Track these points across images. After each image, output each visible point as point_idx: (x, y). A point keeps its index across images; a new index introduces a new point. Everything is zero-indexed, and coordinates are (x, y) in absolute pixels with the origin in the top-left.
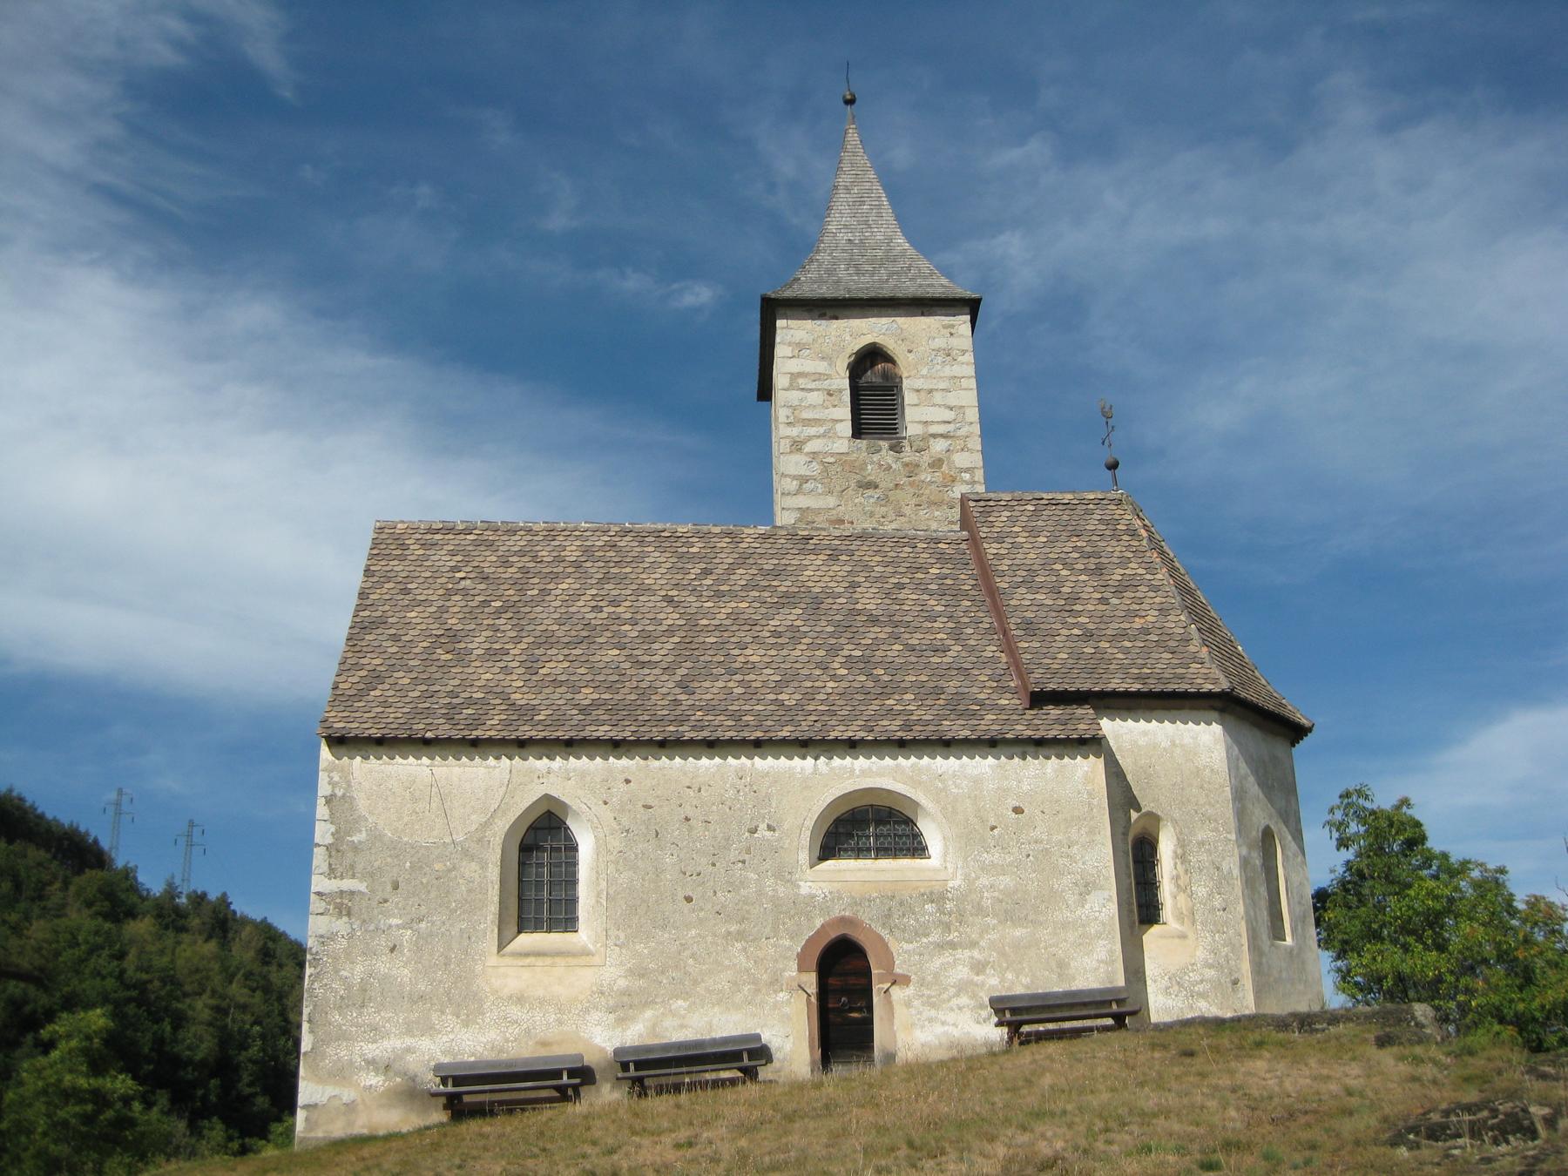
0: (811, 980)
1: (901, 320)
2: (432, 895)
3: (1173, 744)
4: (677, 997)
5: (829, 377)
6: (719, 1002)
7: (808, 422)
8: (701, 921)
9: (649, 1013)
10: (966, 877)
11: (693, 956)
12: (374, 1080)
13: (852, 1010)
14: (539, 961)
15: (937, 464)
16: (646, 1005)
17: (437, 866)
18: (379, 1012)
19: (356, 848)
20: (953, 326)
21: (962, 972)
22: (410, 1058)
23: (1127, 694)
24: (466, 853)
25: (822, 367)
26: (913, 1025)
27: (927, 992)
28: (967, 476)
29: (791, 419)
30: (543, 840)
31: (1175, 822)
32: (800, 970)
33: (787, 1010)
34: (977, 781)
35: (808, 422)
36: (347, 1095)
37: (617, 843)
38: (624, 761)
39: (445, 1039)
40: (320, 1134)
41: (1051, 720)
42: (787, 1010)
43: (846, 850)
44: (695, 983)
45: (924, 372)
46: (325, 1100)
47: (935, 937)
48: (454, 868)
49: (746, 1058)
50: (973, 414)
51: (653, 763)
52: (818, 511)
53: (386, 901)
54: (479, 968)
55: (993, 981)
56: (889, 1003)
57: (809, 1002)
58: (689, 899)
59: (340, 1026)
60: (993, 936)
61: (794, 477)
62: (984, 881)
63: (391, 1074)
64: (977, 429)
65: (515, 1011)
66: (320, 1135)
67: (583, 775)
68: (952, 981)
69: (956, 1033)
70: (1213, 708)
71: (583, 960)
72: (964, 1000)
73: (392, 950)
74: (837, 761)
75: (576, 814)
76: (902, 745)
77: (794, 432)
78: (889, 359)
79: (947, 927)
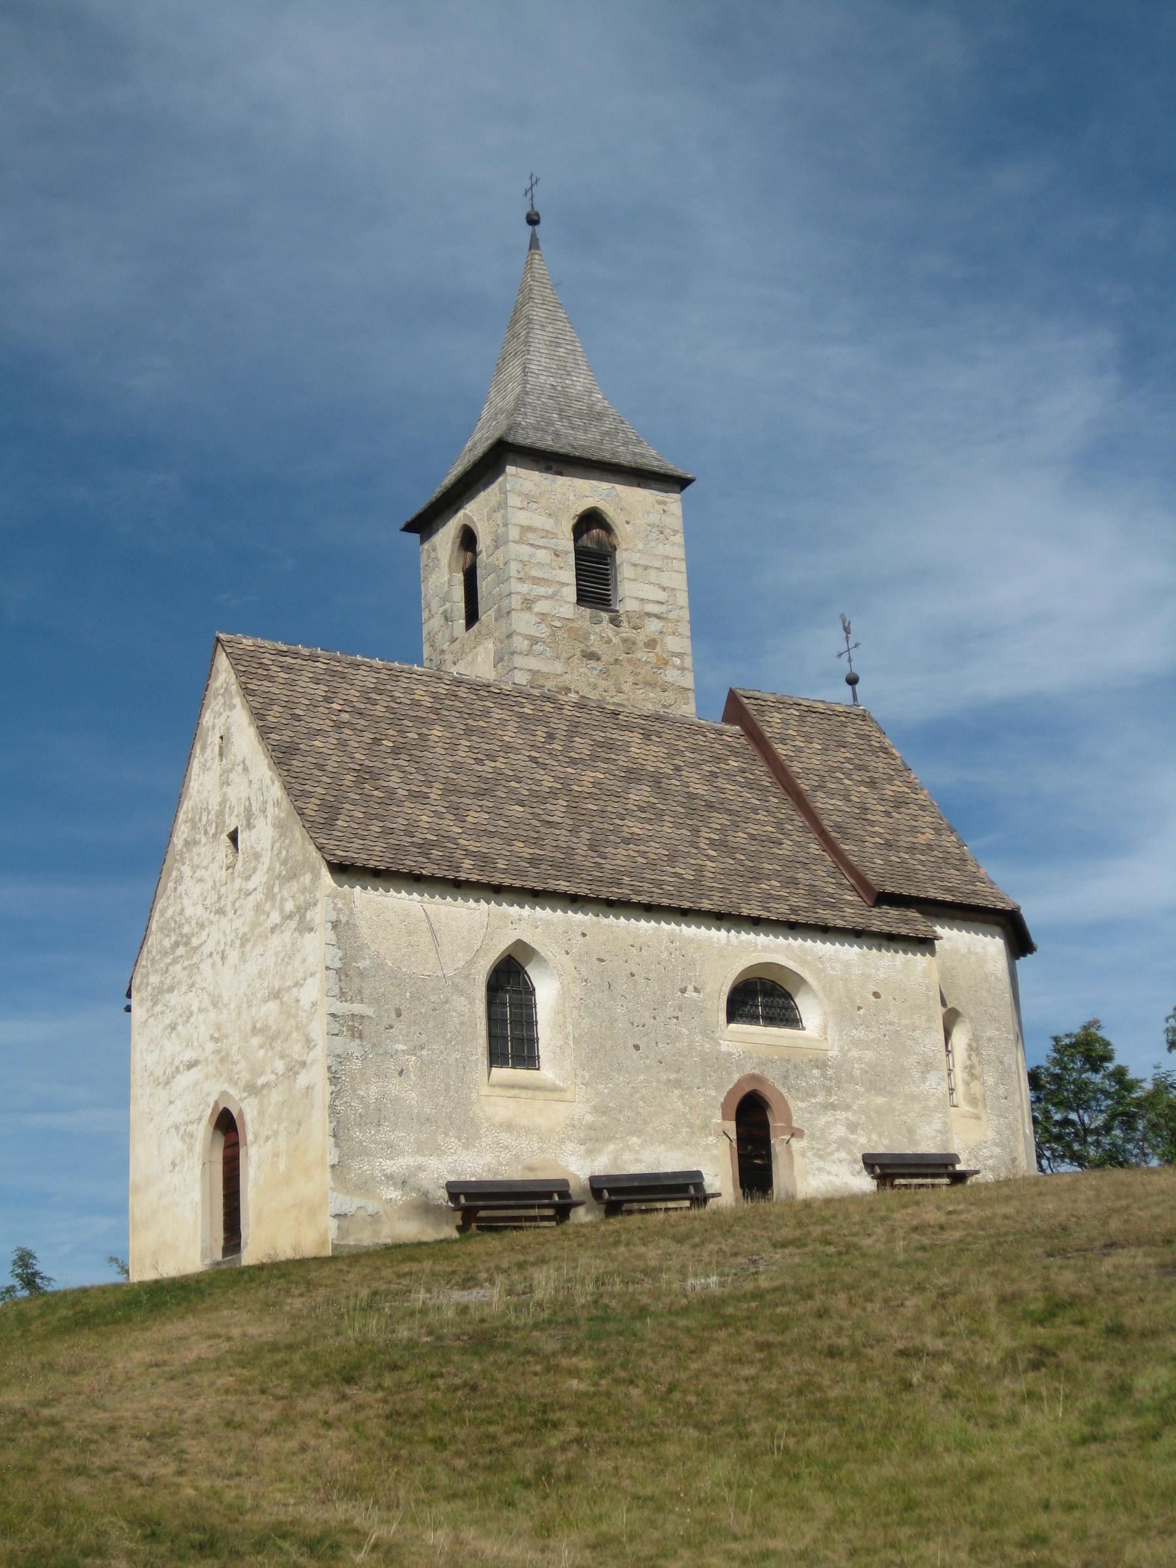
0: (731, 1127)
1: (620, 488)
2: (430, 1025)
3: (969, 952)
4: (632, 1134)
5: (555, 536)
6: (664, 1141)
7: (537, 581)
8: (648, 1068)
9: (611, 1147)
10: (841, 1048)
11: (642, 1098)
12: (393, 1194)
13: (756, 1157)
14: (523, 1094)
15: (651, 644)
16: (609, 1139)
17: (433, 998)
18: (393, 1131)
19: (361, 974)
20: (665, 503)
21: (840, 1131)
22: (422, 1175)
23: (944, 904)
24: (455, 986)
25: (549, 524)
26: (807, 1172)
27: (817, 1146)
28: (677, 661)
29: (521, 575)
30: (509, 980)
31: (971, 1019)
32: (724, 1118)
33: (715, 1152)
34: (847, 965)
35: (537, 581)
36: (372, 1206)
37: (578, 991)
38: (580, 916)
39: (450, 1159)
40: (351, 1242)
41: (889, 919)
42: (715, 1152)
43: (741, 1016)
44: (645, 1122)
45: (641, 546)
46: (353, 1210)
47: (820, 1099)
48: (447, 1002)
49: (685, 1187)
50: (683, 599)
51: (604, 921)
52: (547, 676)
53: (391, 1027)
54: (474, 1096)
55: (863, 1140)
56: (790, 1153)
57: (731, 1145)
58: (637, 1047)
59: (361, 1142)
60: (862, 1102)
61: (526, 637)
62: (854, 1053)
63: (407, 1189)
64: (686, 614)
65: (505, 1138)
66: (352, 1243)
67: (548, 924)
68: (833, 1137)
69: (838, 1182)
70: (998, 924)
71: (557, 1095)
72: (843, 1155)
73: (401, 1073)
74: (743, 936)
75: (543, 961)
76: (792, 927)
77: (524, 588)
78: (607, 527)
79: (829, 1091)
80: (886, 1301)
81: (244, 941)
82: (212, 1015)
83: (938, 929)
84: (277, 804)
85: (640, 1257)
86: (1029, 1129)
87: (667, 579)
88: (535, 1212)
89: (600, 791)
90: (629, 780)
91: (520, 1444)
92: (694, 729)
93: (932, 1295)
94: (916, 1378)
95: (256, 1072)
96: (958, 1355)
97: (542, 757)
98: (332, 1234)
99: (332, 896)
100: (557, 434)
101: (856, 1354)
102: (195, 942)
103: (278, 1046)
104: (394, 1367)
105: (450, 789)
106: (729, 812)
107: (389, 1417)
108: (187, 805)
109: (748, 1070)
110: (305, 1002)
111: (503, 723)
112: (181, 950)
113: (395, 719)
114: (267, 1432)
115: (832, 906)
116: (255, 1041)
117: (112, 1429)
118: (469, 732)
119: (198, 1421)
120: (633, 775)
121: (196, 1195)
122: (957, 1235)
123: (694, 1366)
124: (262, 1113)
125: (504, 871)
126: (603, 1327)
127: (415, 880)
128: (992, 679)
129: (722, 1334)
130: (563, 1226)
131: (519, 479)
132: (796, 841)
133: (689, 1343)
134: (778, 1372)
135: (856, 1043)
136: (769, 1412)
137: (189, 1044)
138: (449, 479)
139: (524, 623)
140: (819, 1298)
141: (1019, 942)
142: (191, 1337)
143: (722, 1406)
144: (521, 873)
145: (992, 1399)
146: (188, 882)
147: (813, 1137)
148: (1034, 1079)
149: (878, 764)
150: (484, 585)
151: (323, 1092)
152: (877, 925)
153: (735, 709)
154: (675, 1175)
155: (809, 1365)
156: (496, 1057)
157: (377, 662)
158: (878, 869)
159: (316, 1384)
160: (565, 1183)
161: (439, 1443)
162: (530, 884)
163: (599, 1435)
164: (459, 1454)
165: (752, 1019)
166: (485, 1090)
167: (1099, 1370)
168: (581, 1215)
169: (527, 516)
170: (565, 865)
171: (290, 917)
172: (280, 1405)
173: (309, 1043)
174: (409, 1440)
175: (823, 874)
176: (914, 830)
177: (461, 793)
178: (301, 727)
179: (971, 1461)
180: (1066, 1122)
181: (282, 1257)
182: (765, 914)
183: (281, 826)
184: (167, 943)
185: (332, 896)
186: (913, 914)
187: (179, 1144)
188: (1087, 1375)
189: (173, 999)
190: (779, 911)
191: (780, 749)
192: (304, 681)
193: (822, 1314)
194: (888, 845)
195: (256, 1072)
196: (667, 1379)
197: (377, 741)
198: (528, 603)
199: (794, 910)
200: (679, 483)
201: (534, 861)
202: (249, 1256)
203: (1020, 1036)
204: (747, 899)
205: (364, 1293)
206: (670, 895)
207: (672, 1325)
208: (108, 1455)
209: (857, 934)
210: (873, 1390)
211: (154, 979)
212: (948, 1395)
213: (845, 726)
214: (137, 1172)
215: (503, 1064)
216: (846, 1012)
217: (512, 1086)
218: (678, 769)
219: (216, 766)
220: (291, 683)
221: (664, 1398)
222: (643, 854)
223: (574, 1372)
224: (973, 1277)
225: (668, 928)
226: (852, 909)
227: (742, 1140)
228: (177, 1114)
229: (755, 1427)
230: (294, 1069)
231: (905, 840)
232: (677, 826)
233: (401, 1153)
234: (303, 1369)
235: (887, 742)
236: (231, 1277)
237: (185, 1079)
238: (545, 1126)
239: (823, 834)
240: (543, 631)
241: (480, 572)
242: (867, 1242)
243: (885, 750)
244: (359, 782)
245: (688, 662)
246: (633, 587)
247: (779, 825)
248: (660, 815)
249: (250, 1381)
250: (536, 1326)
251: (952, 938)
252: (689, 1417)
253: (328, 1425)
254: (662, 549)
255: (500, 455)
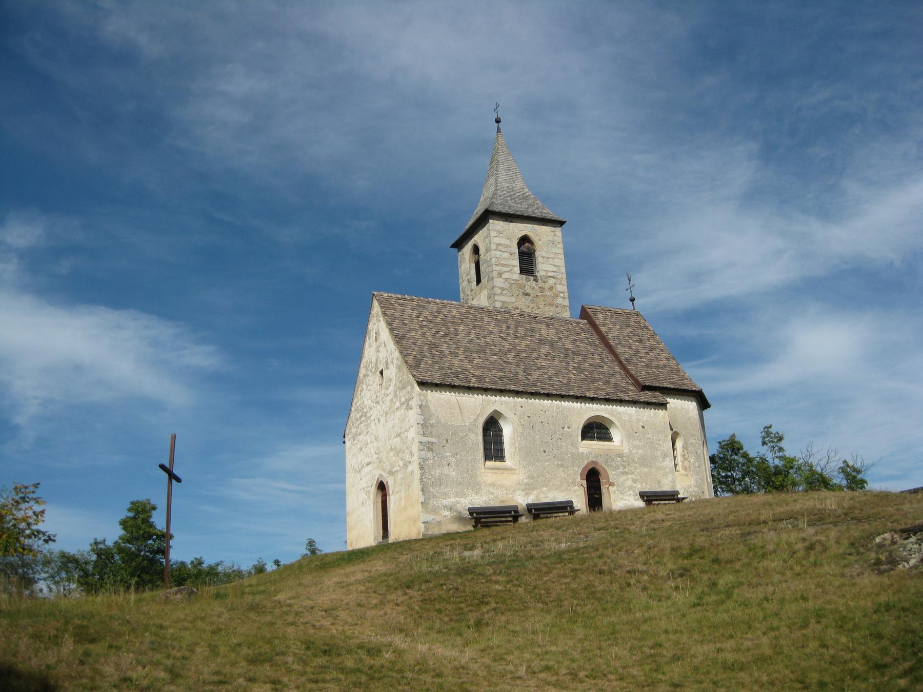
1: (536, 226)
7: (503, 265)
9: (535, 492)
12: (447, 513)
15: (551, 288)
16: (534, 489)
19: (432, 426)
21: (630, 483)
25: (507, 242)
30: (492, 426)
34: (630, 415)
35: (503, 265)
36: (438, 518)
49: (566, 507)
50: (563, 270)
52: (508, 303)
55: (639, 486)
62: (635, 451)
64: (565, 276)
65: (492, 489)
67: (507, 403)
69: (629, 503)
72: (631, 492)
74: (587, 405)
76: (607, 401)
77: (498, 268)
78: (531, 243)
79: (625, 467)
80: (627, 551)
81: (387, 414)
82: (375, 444)
83: (668, 400)
84: (397, 359)
85: (541, 536)
86: (710, 479)
87: (556, 262)
88: (504, 519)
89: (528, 348)
90: (540, 344)
91: (471, 611)
92: (568, 322)
93: (645, 548)
94: (633, 581)
95: (392, 466)
96: (651, 572)
97: (505, 336)
98: (422, 530)
99: (419, 395)
100: (510, 206)
101: (610, 573)
102: (368, 415)
103: (400, 455)
104: (427, 581)
105: (467, 350)
106: (582, 355)
107: (422, 601)
108: (364, 361)
109: (591, 459)
110: (410, 438)
111: (489, 323)
112: (363, 418)
113: (445, 323)
114: (373, 608)
115: (624, 392)
116: (392, 454)
117: (312, 608)
118: (475, 327)
119: (347, 604)
120: (542, 342)
121: (371, 516)
122: (669, 524)
123: (545, 579)
124: (395, 482)
125: (488, 383)
126: (512, 565)
127: (452, 387)
128: (710, 291)
129: (559, 566)
130: (517, 525)
131: (495, 225)
132: (610, 366)
133: (544, 569)
134: (578, 580)
135: (635, 447)
136: (572, 597)
137: (367, 456)
138: (467, 227)
139: (498, 282)
140: (601, 550)
141: (703, 404)
142: (357, 572)
143: (554, 595)
144: (496, 383)
145: (661, 590)
146: (365, 391)
147: (618, 486)
148: (712, 459)
149: (643, 333)
150: (482, 268)
151: (417, 473)
152: (642, 399)
153: (584, 314)
154: (562, 502)
155: (591, 578)
156: (487, 457)
157: (438, 301)
158: (643, 376)
159: (396, 589)
160: (517, 507)
161: (439, 611)
162: (499, 387)
163: (504, 607)
164: (446, 615)
165: (593, 438)
166: (483, 470)
167: (705, 577)
168: (523, 520)
169: (499, 239)
170: (514, 379)
171: (403, 404)
172: (381, 597)
173: (412, 454)
174: (428, 610)
175: (621, 379)
176: (658, 360)
177: (472, 352)
178: (407, 328)
179: (647, 615)
180: (727, 476)
181: (401, 539)
182: (596, 396)
183: (399, 367)
184: (358, 416)
185: (419, 395)
186: (657, 394)
187: (365, 496)
188: (701, 579)
189: (361, 438)
190: (602, 394)
191: (603, 329)
192: (408, 310)
193: (601, 557)
194: (647, 366)
195: (392, 466)
196: (533, 584)
197: (437, 332)
198: (500, 275)
199: (608, 394)
200: (560, 223)
201: (501, 378)
202: (391, 539)
203: (705, 442)
204: (589, 390)
205: (431, 553)
206: (557, 390)
207: (540, 563)
208: (307, 617)
209: (634, 403)
210: (615, 586)
211: (354, 430)
212: (644, 589)
213: (631, 319)
214: (349, 507)
215: (491, 460)
216: (631, 434)
217: (494, 469)
218: (560, 338)
219: (374, 345)
220: (402, 311)
221: (530, 592)
222: (546, 373)
223: (497, 582)
224: (663, 541)
225: (556, 403)
226: (632, 393)
227: (589, 487)
228: (363, 484)
229: (566, 603)
230: (407, 464)
231: (654, 364)
232: (560, 361)
233: (449, 497)
234: (392, 583)
235: (647, 324)
236: (386, 547)
237: (366, 470)
238: (508, 484)
239: (620, 362)
240: (507, 285)
241: (481, 263)
242: (632, 528)
243: (646, 327)
244: (430, 349)
245: (566, 295)
246: (542, 266)
247: (602, 360)
248: (553, 358)
249: (370, 588)
250: (488, 565)
251: (674, 403)
252: (540, 600)
253: (398, 605)
254: (554, 250)
255: (487, 216)
